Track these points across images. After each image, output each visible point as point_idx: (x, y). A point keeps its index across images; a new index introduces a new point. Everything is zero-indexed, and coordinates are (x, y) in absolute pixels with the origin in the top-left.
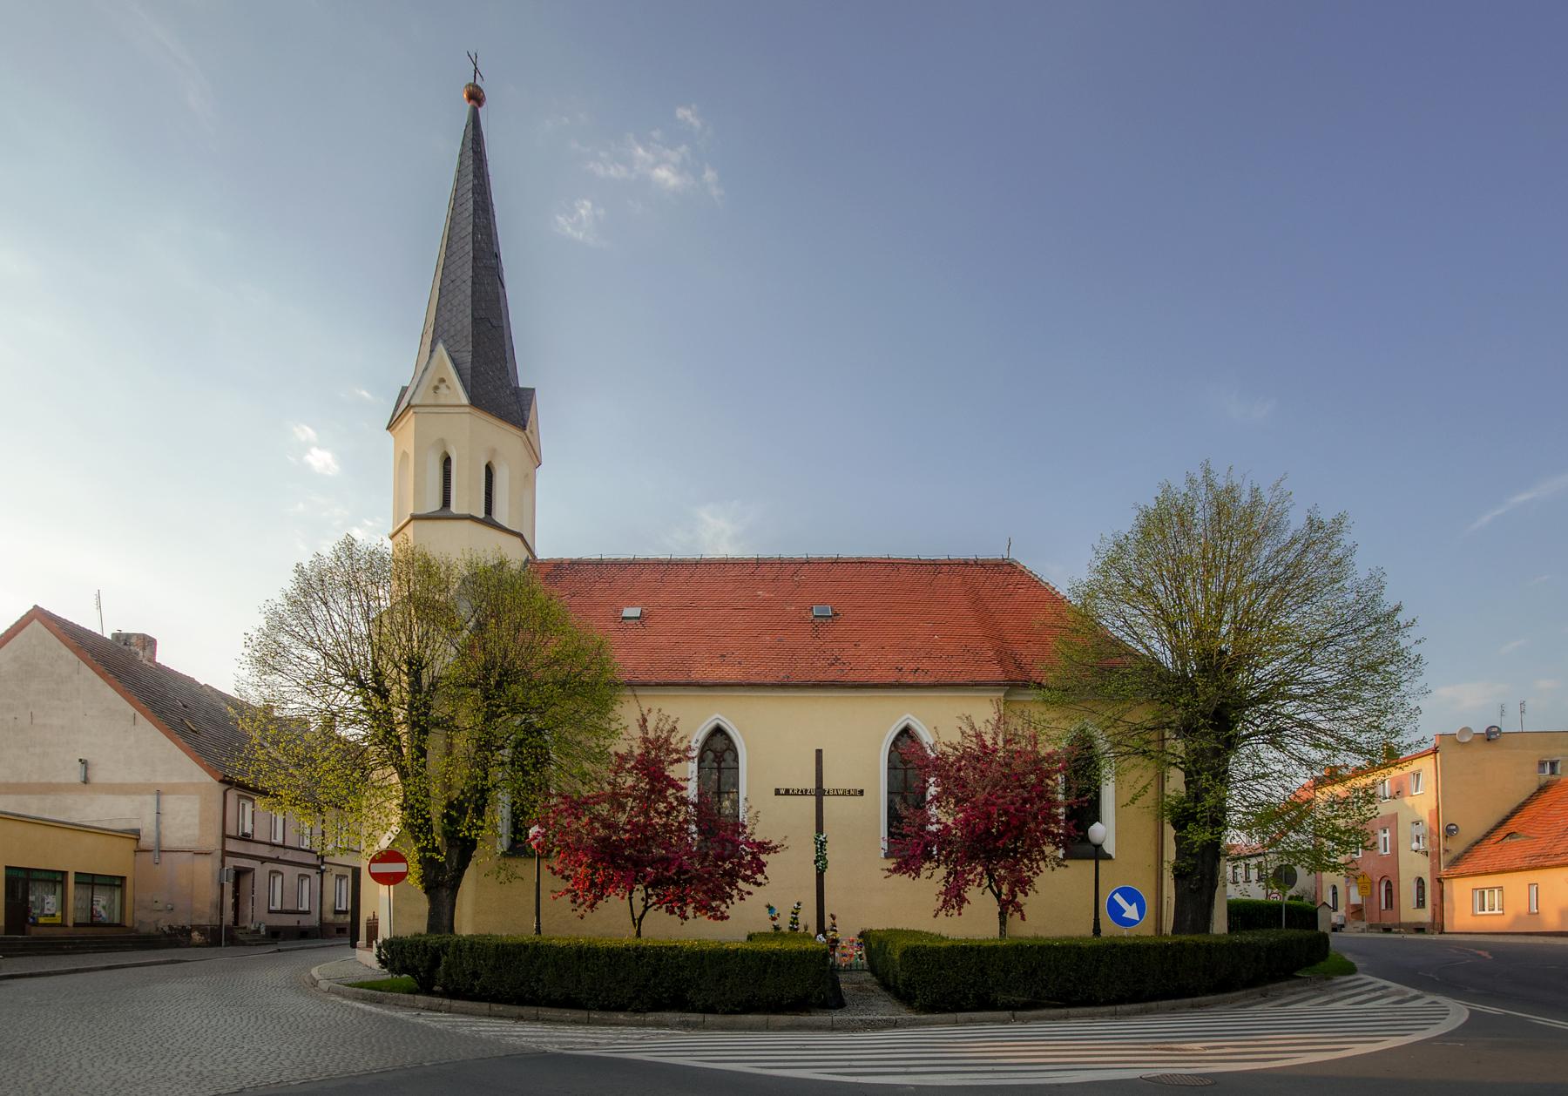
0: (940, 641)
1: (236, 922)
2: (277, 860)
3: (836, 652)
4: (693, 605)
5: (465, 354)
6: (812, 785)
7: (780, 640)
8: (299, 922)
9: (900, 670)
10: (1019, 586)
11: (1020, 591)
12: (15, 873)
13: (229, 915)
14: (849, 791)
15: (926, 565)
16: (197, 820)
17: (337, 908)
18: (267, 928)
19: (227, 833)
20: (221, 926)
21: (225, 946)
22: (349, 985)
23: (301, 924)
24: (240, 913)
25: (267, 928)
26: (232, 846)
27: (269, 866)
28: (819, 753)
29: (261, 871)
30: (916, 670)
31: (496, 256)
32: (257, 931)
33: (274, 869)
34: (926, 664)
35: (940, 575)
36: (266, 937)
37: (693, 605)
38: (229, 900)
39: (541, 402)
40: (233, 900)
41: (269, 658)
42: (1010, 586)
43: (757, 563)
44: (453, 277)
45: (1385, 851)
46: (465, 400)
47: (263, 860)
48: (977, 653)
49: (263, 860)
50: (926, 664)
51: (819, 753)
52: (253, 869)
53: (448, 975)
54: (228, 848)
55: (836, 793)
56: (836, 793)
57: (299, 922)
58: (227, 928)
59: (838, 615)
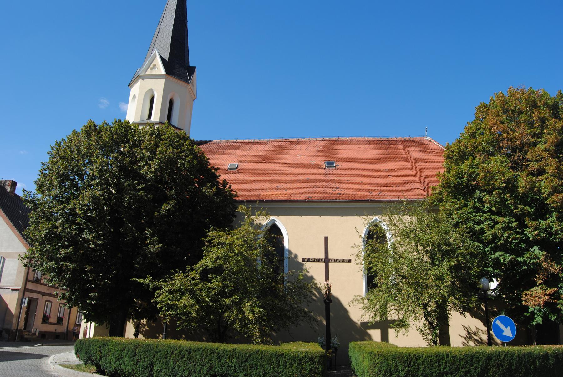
0: (392, 178)
1: (25, 329)
2: (50, 295)
3: (337, 185)
4: (264, 162)
5: (166, 54)
6: (323, 257)
7: (308, 179)
8: (56, 330)
9: (371, 193)
10: (432, 150)
11: (434, 153)
12: (31, 299)
13: (22, 324)
14: (332, 260)
15: (384, 141)
16: (15, 272)
17: (77, 323)
18: (40, 332)
19: (29, 279)
20: (17, 330)
21: (17, 341)
22: (63, 366)
23: (57, 331)
24: (28, 323)
25: (40, 332)
26: (30, 286)
27: (46, 298)
28: (326, 239)
29: (42, 300)
30: (380, 194)
31: (185, 16)
32: (35, 334)
33: (49, 299)
34: (385, 190)
35: (391, 145)
36: (38, 337)
37: (264, 162)
38: (23, 316)
39: (197, 72)
40: (25, 316)
41: (40, 187)
42: (427, 151)
43: (298, 141)
44: (166, 25)
45: (47, 304)
46: (163, 72)
47: (43, 294)
48: (412, 184)
49: (43, 294)
50: (385, 190)
51: (326, 239)
52: (38, 299)
53: (363, 344)
54: (27, 287)
55: (336, 261)
56: (336, 261)
57: (56, 330)
58: (20, 331)
59: (338, 165)
